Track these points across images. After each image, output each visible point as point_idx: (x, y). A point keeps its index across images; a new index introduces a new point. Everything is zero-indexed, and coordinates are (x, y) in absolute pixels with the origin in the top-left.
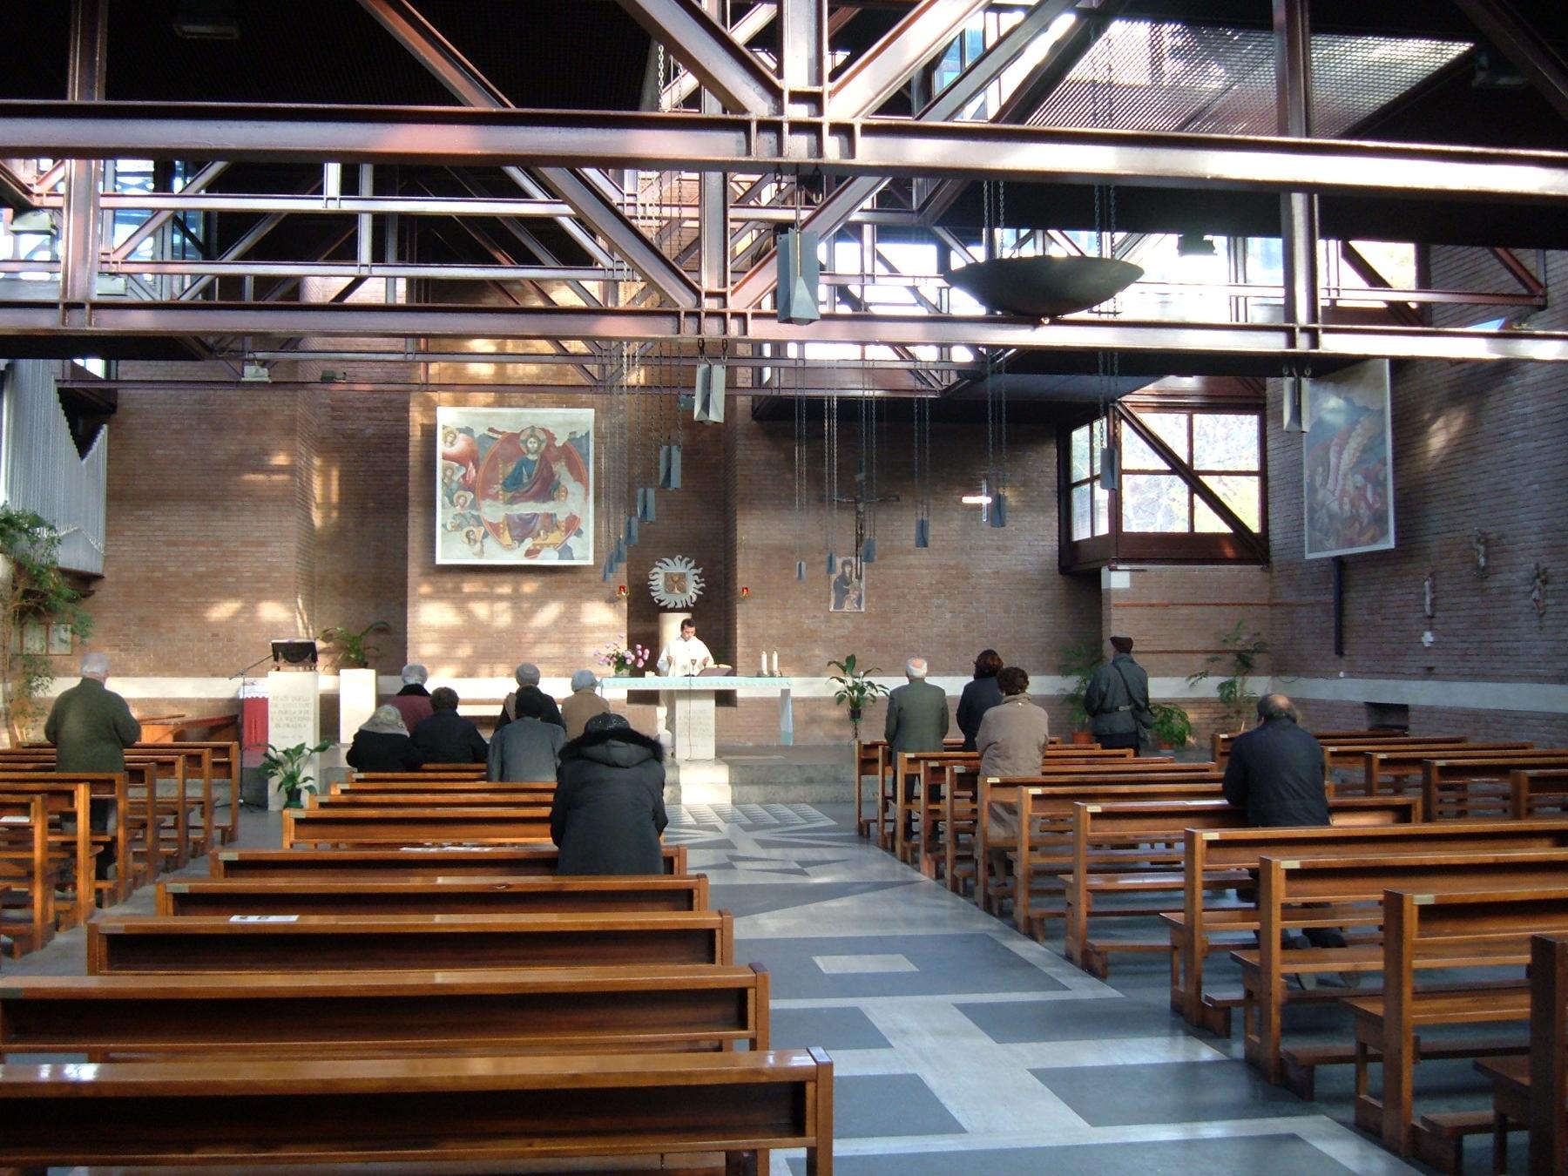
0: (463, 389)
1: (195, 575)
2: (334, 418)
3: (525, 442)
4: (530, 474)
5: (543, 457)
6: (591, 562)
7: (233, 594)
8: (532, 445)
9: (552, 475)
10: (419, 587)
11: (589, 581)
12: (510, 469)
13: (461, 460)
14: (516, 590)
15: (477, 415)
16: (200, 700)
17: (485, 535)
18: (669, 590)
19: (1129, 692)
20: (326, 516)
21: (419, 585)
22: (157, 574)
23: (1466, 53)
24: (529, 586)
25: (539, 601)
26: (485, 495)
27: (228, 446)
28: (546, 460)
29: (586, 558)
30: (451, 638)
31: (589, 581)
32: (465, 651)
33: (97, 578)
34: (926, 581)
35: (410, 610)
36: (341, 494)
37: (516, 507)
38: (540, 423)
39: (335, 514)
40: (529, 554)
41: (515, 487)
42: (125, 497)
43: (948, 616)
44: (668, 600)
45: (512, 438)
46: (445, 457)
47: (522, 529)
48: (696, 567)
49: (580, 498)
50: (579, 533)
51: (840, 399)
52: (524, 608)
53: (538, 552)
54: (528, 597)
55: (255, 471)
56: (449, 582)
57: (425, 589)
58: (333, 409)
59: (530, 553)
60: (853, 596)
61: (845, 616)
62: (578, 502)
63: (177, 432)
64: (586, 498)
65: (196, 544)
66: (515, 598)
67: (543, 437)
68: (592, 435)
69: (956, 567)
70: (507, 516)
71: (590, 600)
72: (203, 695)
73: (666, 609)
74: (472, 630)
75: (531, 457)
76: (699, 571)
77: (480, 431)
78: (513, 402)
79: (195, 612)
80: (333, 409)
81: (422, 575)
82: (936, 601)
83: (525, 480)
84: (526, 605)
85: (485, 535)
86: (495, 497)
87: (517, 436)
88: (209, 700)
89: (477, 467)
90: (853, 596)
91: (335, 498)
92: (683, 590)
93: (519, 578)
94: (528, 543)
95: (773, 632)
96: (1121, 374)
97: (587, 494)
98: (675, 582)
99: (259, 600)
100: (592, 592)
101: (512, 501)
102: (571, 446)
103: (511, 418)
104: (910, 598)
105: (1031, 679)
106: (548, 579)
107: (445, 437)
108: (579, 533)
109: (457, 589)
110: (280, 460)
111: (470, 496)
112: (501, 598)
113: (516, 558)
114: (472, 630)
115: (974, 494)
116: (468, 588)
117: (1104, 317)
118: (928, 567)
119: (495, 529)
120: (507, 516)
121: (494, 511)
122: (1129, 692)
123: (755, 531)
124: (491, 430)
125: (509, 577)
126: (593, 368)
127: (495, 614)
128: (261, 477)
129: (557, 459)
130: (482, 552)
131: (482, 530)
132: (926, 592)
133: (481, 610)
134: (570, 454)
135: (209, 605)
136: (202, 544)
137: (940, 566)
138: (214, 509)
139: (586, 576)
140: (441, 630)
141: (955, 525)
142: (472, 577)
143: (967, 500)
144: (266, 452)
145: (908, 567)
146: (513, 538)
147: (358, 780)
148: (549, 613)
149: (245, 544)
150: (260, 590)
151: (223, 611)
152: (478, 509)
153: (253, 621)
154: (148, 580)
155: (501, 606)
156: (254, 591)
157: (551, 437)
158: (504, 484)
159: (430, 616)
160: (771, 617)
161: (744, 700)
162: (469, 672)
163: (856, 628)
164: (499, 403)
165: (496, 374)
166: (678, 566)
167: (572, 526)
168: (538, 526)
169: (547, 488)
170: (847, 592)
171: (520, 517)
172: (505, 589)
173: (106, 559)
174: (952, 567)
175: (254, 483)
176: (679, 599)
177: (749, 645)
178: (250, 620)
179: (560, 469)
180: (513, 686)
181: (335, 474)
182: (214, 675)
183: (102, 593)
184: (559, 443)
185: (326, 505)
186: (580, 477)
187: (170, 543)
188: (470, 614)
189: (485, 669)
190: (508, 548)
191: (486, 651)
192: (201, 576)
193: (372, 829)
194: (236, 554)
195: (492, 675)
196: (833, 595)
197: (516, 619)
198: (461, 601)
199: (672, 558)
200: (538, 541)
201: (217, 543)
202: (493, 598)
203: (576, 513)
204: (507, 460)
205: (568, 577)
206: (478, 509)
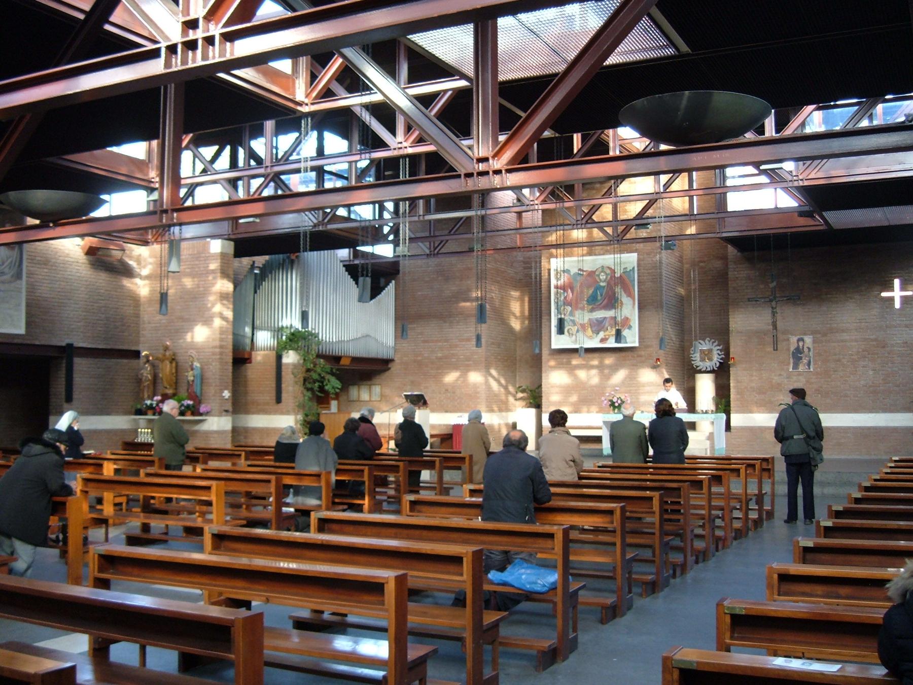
1: (437, 358)
2: (525, 268)
3: (598, 276)
4: (603, 293)
5: (609, 284)
6: (637, 345)
7: (455, 368)
8: (603, 277)
10: (549, 362)
11: (641, 356)
12: (591, 292)
13: (564, 288)
14: (601, 362)
15: (572, 262)
17: (578, 331)
18: (703, 360)
19: (801, 426)
20: (522, 323)
21: (548, 361)
22: (419, 358)
23: (412, 34)
24: (609, 360)
25: (615, 368)
26: (576, 308)
27: (451, 288)
29: (634, 342)
30: (567, 390)
31: (641, 356)
32: (574, 398)
33: (392, 360)
34: (854, 350)
35: (543, 375)
36: (530, 309)
39: (527, 322)
40: (602, 341)
41: (594, 302)
43: (871, 373)
44: (702, 365)
45: (592, 274)
46: (557, 287)
47: (597, 327)
48: (719, 345)
49: (630, 307)
50: (630, 327)
51: (373, 264)
53: (607, 339)
56: (564, 358)
57: (552, 363)
60: (805, 361)
61: (800, 374)
62: (629, 309)
64: (633, 307)
65: (437, 341)
66: (601, 367)
67: (608, 271)
68: (636, 269)
69: (876, 340)
70: (590, 319)
71: (643, 367)
75: (602, 284)
77: (574, 271)
78: (597, 252)
79: (438, 377)
81: (550, 354)
82: (862, 363)
83: (599, 298)
84: (606, 371)
86: (583, 309)
87: (593, 272)
89: (572, 292)
90: (805, 361)
91: (527, 313)
92: (710, 359)
93: (603, 355)
94: (602, 335)
95: (753, 385)
96: (311, 250)
97: (634, 304)
98: (706, 355)
99: (468, 371)
100: (643, 362)
101: (592, 310)
102: (624, 276)
103: (592, 262)
104: (845, 361)
106: (618, 355)
108: (630, 327)
109: (569, 363)
111: (569, 308)
112: (592, 367)
113: (594, 343)
114: (578, 386)
115: (888, 291)
116: (575, 362)
118: (856, 341)
119: (583, 327)
120: (590, 319)
121: (584, 316)
122: (801, 426)
124: (580, 270)
125: (596, 355)
126: (609, 230)
127: (589, 376)
131: (576, 328)
132: (855, 357)
133: (582, 374)
135: (443, 374)
137: (865, 340)
138: (445, 322)
140: (560, 386)
141: (875, 312)
142: (609, 354)
143: (884, 294)
145: (842, 341)
147: (887, 473)
148: (620, 376)
149: (462, 340)
150: (468, 366)
151: (451, 377)
152: (574, 316)
155: (594, 372)
156: (465, 366)
158: (588, 301)
160: (752, 376)
163: (807, 382)
164: (590, 254)
166: (704, 346)
168: (607, 325)
169: (612, 302)
170: (801, 358)
171: (597, 320)
173: (396, 351)
174: (872, 340)
175: (464, 307)
176: (708, 365)
177: (738, 393)
178: (464, 382)
179: (618, 290)
180: (401, 420)
181: (526, 299)
182: (446, 412)
183: (395, 368)
184: (618, 275)
186: (630, 295)
187: (425, 342)
189: (585, 409)
190: (590, 338)
192: (441, 358)
193: (197, 492)
194: (456, 346)
195: (588, 412)
196: (792, 361)
197: (601, 379)
198: (571, 369)
199: (704, 340)
200: (607, 333)
201: (447, 341)
203: (628, 315)
204: (589, 287)
205: (629, 354)
206: (574, 316)
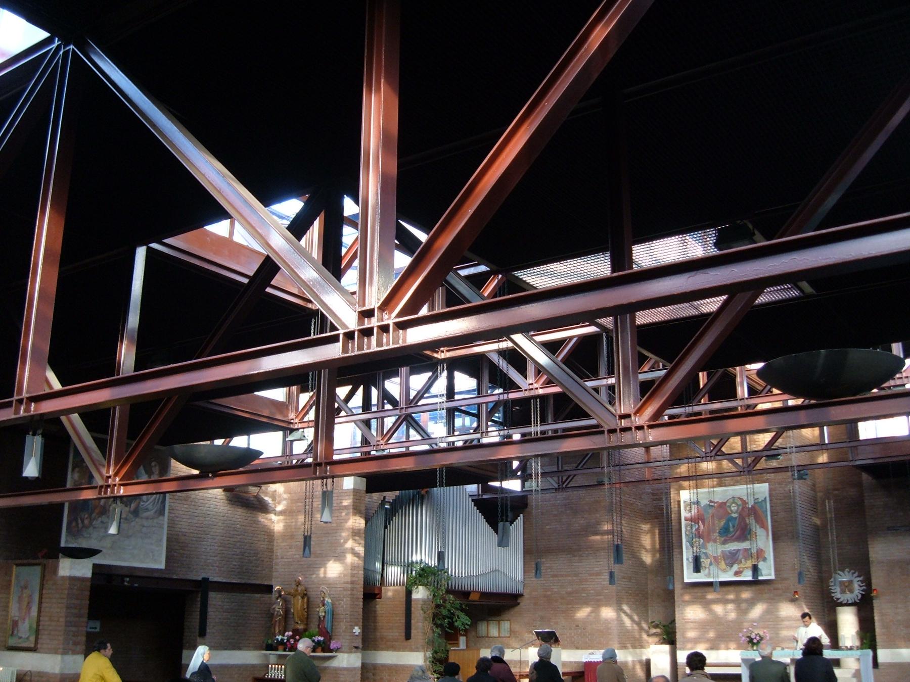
0: (696, 478)
3: (730, 507)
4: (736, 525)
5: (740, 515)
6: (773, 577)
7: (586, 603)
9: (746, 525)
11: (777, 589)
12: (722, 523)
16: (571, 662)
17: (711, 564)
24: (746, 594)
25: (752, 603)
26: (709, 540)
27: (579, 522)
28: (742, 517)
29: (770, 575)
30: (703, 626)
31: (777, 589)
32: (711, 634)
33: (521, 595)
37: (727, 546)
38: (737, 495)
39: (658, 555)
41: (726, 534)
42: (534, 554)
45: (723, 505)
46: (686, 519)
47: (732, 559)
48: (859, 576)
49: (764, 538)
50: (765, 559)
52: (743, 608)
54: (746, 601)
55: (596, 534)
58: (653, 494)
59: (737, 573)
62: (764, 541)
63: (555, 515)
64: (767, 538)
65: (566, 576)
66: (737, 602)
67: (740, 502)
68: (768, 499)
72: (572, 660)
73: (842, 605)
74: (715, 622)
75: (734, 515)
76: (861, 579)
77: (704, 502)
80: (653, 494)
84: (744, 606)
85: (711, 564)
86: (715, 541)
87: (725, 503)
88: (576, 662)
89: (704, 524)
91: (657, 546)
92: (851, 591)
93: (738, 588)
94: (736, 567)
95: (900, 618)
97: (768, 535)
100: (781, 595)
101: (724, 542)
103: (722, 493)
105: (482, 656)
107: (685, 508)
108: (765, 559)
109: (703, 597)
110: (606, 527)
114: (715, 622)
116: (710, 596)
117: (889, 392)
123: (881, 551)
124: (711, 501)
127: (725, 611)
128: (598, 537)
129: (749, 516)
130: (709, 573)
133: (718, 609)
134: (754, 511)
135: (575, 610)
136: (569, 576)
138: (574, 556)
139: (776, 586)
144: (599, 523)
146: (727, 565)
148: (758, 610)
149: (591, 575)
150: (598, 600)
151: (583, 613)
152: (706, 548)
153: (598, 618)
154: (545, 596)
155: (730, 606)
156: (597, 602)
157: (744, 502)
158: (719, 533)
159: (691, 614)
161: (883, 664)
162: (714, 647)
165: (717, 468)
167: (760, 555)
168: (741, 557)
171: (730, 552)
172: (731, 597)
176: (848, 597)
179: (751, 521)
181: (657, 531)
182: (577, 648)
183: (524, 603)
185: (653, 551)
186: (763, 526)
187: (554, 576)
188: (711, 611)
190: (724, 571)
191: (723, 635)
192: (569, 593)
195: (728, 649)
198: (706, 605)
200: (741, 566)
201: (576, 575)
202: (726, 602)
204: (720, 519)
205: (766, 587)
206: (706, 548)
